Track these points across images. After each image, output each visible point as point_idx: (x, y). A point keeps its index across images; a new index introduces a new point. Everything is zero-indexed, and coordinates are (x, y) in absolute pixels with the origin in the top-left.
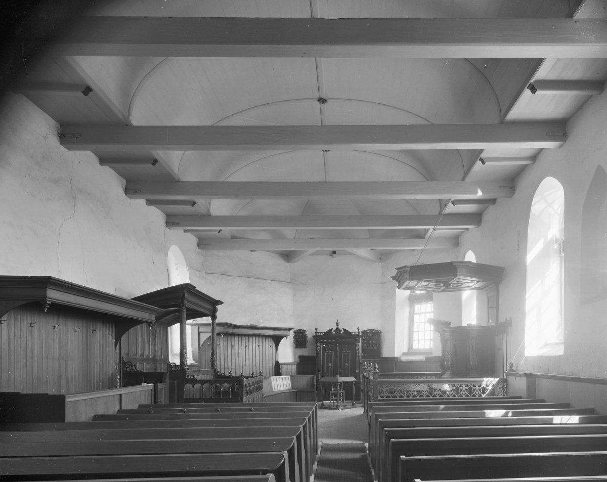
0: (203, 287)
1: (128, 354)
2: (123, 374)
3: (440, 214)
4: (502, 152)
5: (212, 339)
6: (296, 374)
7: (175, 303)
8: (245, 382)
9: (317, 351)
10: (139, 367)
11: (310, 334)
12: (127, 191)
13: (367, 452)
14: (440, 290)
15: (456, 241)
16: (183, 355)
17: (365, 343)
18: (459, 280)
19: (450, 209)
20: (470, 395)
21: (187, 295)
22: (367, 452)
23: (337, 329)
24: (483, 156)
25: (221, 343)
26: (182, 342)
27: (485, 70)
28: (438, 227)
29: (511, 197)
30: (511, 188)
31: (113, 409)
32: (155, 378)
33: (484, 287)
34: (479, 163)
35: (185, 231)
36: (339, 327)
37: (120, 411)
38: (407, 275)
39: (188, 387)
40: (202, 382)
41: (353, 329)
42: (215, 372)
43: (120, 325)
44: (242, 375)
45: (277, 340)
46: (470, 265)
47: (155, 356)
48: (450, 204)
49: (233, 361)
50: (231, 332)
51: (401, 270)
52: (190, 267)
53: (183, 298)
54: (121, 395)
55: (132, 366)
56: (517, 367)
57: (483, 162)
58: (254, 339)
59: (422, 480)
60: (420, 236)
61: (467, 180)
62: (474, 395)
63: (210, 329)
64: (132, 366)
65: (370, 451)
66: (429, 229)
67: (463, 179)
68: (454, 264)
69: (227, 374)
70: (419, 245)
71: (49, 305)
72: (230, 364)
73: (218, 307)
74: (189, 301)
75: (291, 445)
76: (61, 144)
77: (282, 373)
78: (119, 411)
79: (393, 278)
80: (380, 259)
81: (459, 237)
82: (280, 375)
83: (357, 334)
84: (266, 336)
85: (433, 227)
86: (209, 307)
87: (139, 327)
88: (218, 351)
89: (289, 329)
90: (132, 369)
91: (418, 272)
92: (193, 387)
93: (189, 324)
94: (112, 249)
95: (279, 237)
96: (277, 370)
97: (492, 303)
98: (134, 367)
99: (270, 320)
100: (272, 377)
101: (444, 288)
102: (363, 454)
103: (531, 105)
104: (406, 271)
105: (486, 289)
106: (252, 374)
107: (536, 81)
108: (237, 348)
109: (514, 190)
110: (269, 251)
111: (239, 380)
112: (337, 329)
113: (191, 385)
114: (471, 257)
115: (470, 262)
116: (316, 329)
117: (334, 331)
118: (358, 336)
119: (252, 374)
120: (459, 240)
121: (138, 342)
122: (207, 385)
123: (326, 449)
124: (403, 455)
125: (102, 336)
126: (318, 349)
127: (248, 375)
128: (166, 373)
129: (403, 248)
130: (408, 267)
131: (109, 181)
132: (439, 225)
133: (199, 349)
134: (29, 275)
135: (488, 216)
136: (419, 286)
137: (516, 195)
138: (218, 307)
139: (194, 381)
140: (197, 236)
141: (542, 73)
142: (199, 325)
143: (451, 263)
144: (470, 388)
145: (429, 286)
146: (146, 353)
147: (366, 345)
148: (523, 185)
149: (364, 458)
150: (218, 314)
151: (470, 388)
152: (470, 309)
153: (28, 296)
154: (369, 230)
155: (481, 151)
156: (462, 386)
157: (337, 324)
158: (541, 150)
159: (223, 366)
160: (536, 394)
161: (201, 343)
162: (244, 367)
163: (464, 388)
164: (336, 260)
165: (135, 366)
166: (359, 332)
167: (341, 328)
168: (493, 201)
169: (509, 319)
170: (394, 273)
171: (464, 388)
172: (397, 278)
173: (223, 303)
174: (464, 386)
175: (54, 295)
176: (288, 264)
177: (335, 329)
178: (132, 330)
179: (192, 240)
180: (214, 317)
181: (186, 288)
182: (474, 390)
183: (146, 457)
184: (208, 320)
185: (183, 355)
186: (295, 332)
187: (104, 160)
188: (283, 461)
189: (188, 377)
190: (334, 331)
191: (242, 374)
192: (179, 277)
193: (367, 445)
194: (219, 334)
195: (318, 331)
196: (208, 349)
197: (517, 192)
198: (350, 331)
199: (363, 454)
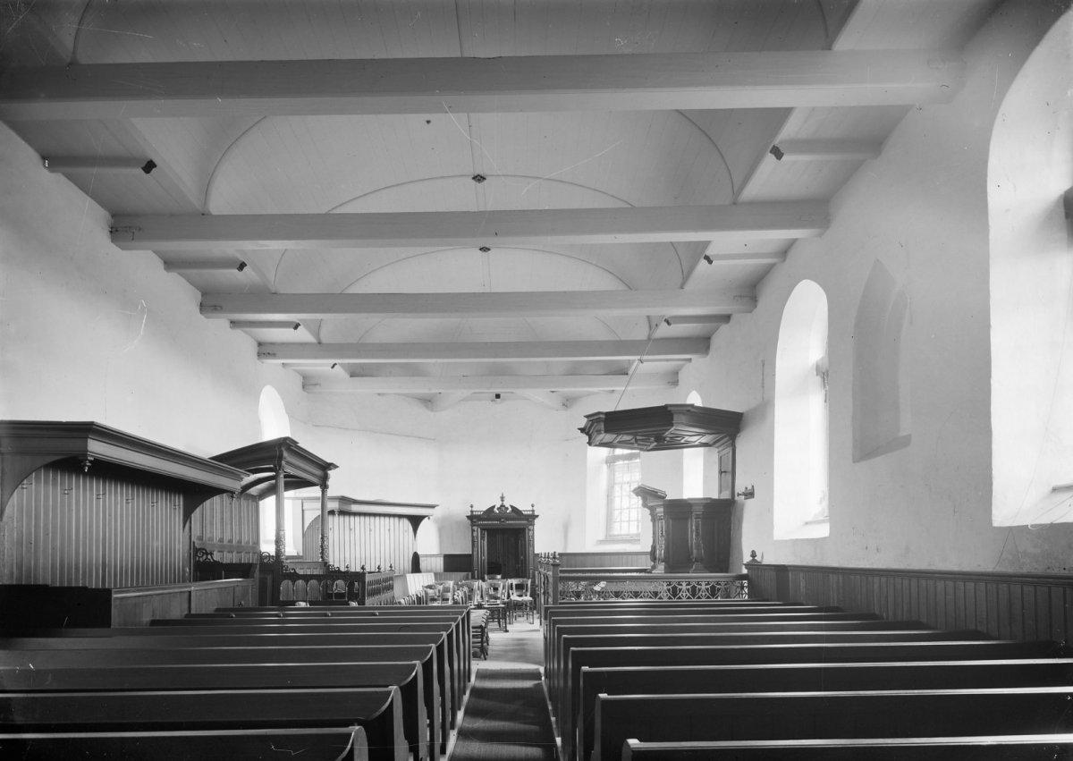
0: (306, 443)
1: (201, 538)
2: (194, 565)
3: (649, 339)
4: (735, 247)
5: (322, 520)
6: (442, 570)
7: (273, 463)
8: (368, 578)
9: (473, 537)
10: (217, 557)
12: (203, 308)
13: (543, 678)
14: (651, 447)
15: (673, 379)
16: (279, 542)
18: (677, 432)
19: (664, 331)
21: (285, 454)
22: (543, 678)
23: (502, 506)
24: (708, 253)
25: (335, 523)
26: (281, 524)
27: (705, 125)
28: (645, 357)
31: (177, 612)
32: (242, 570)
33: (715, 443)
34: (770, 158)
37: (189, 615)
39: (285, 585)
40: (307, 578)
42: (325, 564)
43: (193, 494)
45: (416, 521)
46: (693, 410)
49: (353, 551)
50: (346, 508)
52: (292, 415)
53: (281, 457)
54: (190, 592)
55: (207, 554)
56: (762, 557)
57: (710, 262)
59: (641, 741)
60: (622, 371)
62: (680, 598)
63: (319, 505)
64: (207, 554)
65: (546, 677)
66: (634, 361)
68: (669, 409)
69: (343, 569)
70: (618, 385)
71: (90, 462)
72: (347, 555)
74: (288, 463)
75: (429, 656)
76: (112, 241)
78: (186, 616)
79: (582, 430)
80: (564, 405)
81: (678, 373)
84: (400, 516)
85: (639, 357)
86: (319, 472)
87: (217, 499)
88: (330, 534)
92: (293, 584)
93: (288, 498)
94: (183, 400)
95: (414, 372)
96: (416, 567)
97: (728, 471)
98: (209, 557)
99: (406, 493)
100: (408, 575)
101: (656, 443)
102: (536, 682)
103: (772, 178)
105: (717, 445)
106: (379, 568)
107: (781, 142)
108: (357, 532)
109: (756, 301)
111: (359, 576)
112: (502, 506)
113: (290, 583)
114: (695, 399)
115: (692, 406)
117: (498, 509)
119: (379, 568)
121: (215, 521)
122: (313, 582)
123: (482, 675)
124: (601, 693)
125: (163, 512)
126: (475, 534)
127: (373, 570)
128: (256, 564)
129: (595, 390)
131: (179, 293)
133: (304, 535)
134: (64, 420)
135: (716, 341)
136: (619, 442)
138: (331, 473)
139: (294, 577)
141: (790, 130)
142: (303, 500)
143: (665, 408)
144: (694, 588)
149: (538, 688)
150: (330, 483)
151: (694, 588)
152: (692, 474)
153: (66, 451)
155: (706, 244)
158: (795, 240)
159: (337, 560)
160: (777, 585)
161: (306, 525)
163: (684, 587)
164: (499, 406)
165: (211, 554)
167: (507, 504)
168: (726, 318)
169: (749, 487)
170: (583, 422)
171: (684, 587)
172: (587, 431)
173: (336, 467)
174: (684, 584)
175: (97, 448)
178: (208, 502)
180: (324, 487)
181: (287, 444)
182: (699, 590)
184: (315, 491)
185: (279, 542)
187: (170, 264)
188: (414, 674)
190: (498, 509)
192: (272, 428)
193: (542, 670)
194: (332, 512)
195: (474, 509)
196: (317, 532)
197: (760, 305)
199: (536, 682)
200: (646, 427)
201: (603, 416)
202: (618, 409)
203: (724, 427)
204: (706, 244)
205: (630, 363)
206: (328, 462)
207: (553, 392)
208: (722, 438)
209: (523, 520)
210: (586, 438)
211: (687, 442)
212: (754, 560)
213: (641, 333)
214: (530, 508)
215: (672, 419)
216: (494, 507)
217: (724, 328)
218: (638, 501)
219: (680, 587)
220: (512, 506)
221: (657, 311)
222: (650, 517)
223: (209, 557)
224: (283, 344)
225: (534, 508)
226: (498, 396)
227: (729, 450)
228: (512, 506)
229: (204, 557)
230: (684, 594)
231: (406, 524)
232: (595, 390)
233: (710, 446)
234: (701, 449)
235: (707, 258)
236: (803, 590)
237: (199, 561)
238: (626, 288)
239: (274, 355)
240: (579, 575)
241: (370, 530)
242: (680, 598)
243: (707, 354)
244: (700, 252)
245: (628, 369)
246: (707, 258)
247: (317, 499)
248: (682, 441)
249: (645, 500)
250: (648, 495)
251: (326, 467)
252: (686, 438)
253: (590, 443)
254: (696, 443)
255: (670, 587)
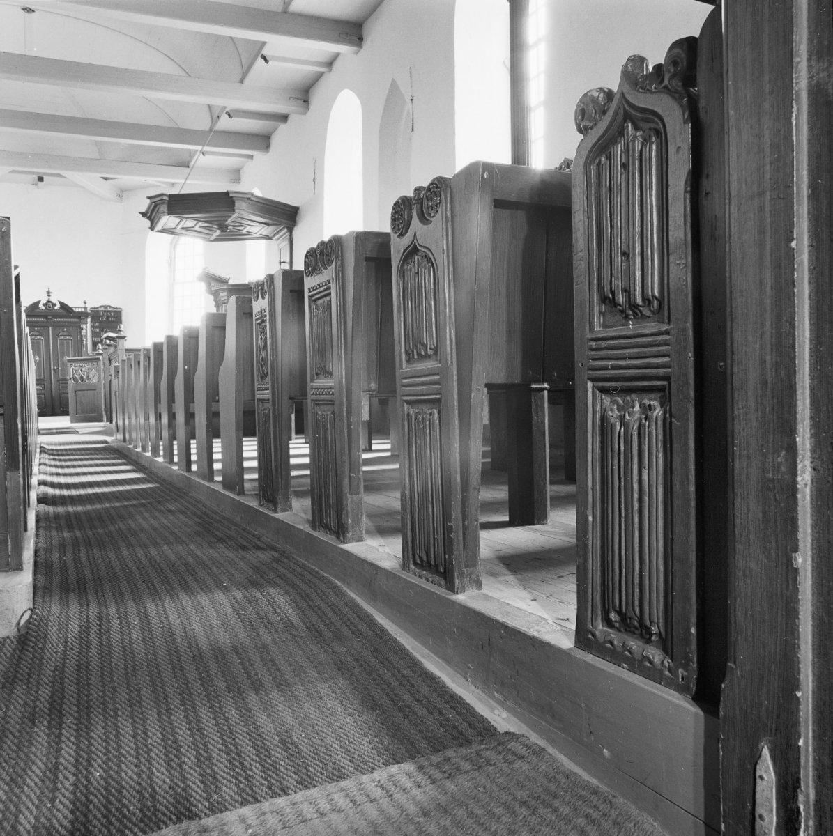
3: (211, 130)
14: (213, 238)
17: (96, 327)
18: (240, 221)
19: (225, 123)
24: (265, 52)
28: (207, 149)
29: (305, 114)
30: (304, 102)
34: (260, 61)
38: (164, 208)
41: (76, 304)
48: (224, 117)
51: (155, 200)
61: (247, 81)
67: (242, 81)
68: (231, 195)
83: (83, 310)
91: (180, 204)
104: (162, 202)
112: (48, 302)
117: (44, 305)
118: (85, 315)
120: (240, 174)
130: (165, 195)
132: (208, 145)
135: (275, 141)
137: (309, 113)
143: (227, 193)
145: (197, 228)
147: (98, 330)
148: (317, 99)
154: (97, 142)
157: (48, 293)
167: (54, 299)
168: (284, 118)
170: (144, 205)
177: (45, 302)
190: (44, 305)
198: (71, 306)
200: (215, 210)
201: (167, 198)
202: (181, 193)
204: (264, 44)
205: (191, 154)
207: (106, 179)
208: (281, 230)
209: (74, 317)
210: (148, 223)
211: (249, 233)
213: (203, 124)
214: (83, 305)
215: (234, 206)
216: (39, 302)
217: (282, 127)
218: (202, 286)
220: (60, 302)
221: (218, 102)
222: (214, 303)
226: (41, 179)
227: (286, 244)
228: (60, 302)
233: (271, 238)
234: (263, 242)
235: (264, 58)
236: (293, 108)
238: (184, 74)
243: (268, 152)
244: (259, 52)
245: (189, 162)
246: (264, 58)
248: (244, 232)
249: (209, 285)
250: (215, 282)
252: (248, 228)
253: (152, 228)
254: (258, 235)
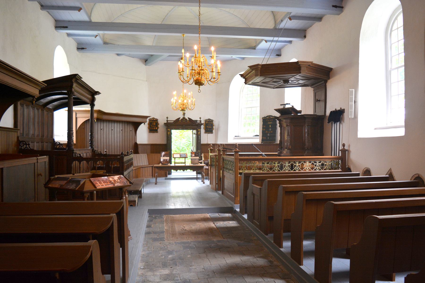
7: (69, 90)
11: (162, 121)
20: (281, 170)
23: (184, 118)
25: (98, 127)
35: (69, 35)
36: (185, 116)
42: (93, 151)
44: (122, 154)
45: (136, 125)
47: (43, 136)
50: (103, 117)
53: (71, 86)
55: (26, 144)
56: (349, 146)
58: (118, 124)
62: (295, 170)
68: (299, 64)
73: (96, 96)
77: (139, 152)
82: (139, 153)
89: (146, 117)
90: (26, 147)
98: (28, 146)
106: (128, 153)
110: (133, 56)
112: (184, 118)
116: (167, 118)
119: (128, 153)
132: (280, 37)
135: (309, 34)
138: (96, 96)
140: (75, 40)
146: (36, 133)
150: (96, 103)
156: (296, 163)
162: (110, 147)
165: (29, 144)
166: (200, 121)
174: (318, 162)
176: (321, 23)
179: (72, 44)
180: (92, 105)
183: (120, 261)
184: (87, 107)
186: (150, 120)
189: (75, 155)
191: (122, 152)
192: (61, 69)
195: (168, 119)
203: (319, 77)
206: (96, 90)
212: (344, 148)
219: (295, 164)
223: (28, 146)
224: (69, 21)
225: (201, 120)
229: (25, 146)
230: (297, 168)
231: (131, 128)
232: (234, 56)
237: (21, 148)
239: (67, 27)
240: (250, 157)
241: (112, 130)
242: (295, 170)
247: (88, 111)
251: (93, 93)
253: (246, 83)
255: (290, 164)
